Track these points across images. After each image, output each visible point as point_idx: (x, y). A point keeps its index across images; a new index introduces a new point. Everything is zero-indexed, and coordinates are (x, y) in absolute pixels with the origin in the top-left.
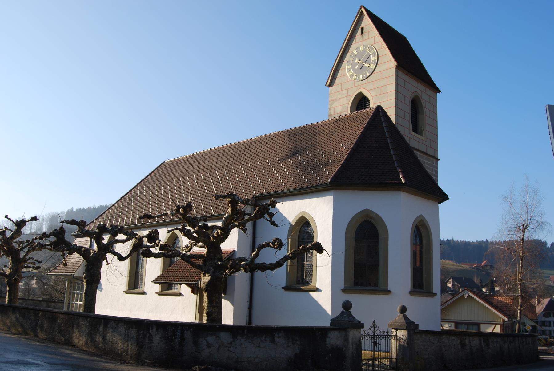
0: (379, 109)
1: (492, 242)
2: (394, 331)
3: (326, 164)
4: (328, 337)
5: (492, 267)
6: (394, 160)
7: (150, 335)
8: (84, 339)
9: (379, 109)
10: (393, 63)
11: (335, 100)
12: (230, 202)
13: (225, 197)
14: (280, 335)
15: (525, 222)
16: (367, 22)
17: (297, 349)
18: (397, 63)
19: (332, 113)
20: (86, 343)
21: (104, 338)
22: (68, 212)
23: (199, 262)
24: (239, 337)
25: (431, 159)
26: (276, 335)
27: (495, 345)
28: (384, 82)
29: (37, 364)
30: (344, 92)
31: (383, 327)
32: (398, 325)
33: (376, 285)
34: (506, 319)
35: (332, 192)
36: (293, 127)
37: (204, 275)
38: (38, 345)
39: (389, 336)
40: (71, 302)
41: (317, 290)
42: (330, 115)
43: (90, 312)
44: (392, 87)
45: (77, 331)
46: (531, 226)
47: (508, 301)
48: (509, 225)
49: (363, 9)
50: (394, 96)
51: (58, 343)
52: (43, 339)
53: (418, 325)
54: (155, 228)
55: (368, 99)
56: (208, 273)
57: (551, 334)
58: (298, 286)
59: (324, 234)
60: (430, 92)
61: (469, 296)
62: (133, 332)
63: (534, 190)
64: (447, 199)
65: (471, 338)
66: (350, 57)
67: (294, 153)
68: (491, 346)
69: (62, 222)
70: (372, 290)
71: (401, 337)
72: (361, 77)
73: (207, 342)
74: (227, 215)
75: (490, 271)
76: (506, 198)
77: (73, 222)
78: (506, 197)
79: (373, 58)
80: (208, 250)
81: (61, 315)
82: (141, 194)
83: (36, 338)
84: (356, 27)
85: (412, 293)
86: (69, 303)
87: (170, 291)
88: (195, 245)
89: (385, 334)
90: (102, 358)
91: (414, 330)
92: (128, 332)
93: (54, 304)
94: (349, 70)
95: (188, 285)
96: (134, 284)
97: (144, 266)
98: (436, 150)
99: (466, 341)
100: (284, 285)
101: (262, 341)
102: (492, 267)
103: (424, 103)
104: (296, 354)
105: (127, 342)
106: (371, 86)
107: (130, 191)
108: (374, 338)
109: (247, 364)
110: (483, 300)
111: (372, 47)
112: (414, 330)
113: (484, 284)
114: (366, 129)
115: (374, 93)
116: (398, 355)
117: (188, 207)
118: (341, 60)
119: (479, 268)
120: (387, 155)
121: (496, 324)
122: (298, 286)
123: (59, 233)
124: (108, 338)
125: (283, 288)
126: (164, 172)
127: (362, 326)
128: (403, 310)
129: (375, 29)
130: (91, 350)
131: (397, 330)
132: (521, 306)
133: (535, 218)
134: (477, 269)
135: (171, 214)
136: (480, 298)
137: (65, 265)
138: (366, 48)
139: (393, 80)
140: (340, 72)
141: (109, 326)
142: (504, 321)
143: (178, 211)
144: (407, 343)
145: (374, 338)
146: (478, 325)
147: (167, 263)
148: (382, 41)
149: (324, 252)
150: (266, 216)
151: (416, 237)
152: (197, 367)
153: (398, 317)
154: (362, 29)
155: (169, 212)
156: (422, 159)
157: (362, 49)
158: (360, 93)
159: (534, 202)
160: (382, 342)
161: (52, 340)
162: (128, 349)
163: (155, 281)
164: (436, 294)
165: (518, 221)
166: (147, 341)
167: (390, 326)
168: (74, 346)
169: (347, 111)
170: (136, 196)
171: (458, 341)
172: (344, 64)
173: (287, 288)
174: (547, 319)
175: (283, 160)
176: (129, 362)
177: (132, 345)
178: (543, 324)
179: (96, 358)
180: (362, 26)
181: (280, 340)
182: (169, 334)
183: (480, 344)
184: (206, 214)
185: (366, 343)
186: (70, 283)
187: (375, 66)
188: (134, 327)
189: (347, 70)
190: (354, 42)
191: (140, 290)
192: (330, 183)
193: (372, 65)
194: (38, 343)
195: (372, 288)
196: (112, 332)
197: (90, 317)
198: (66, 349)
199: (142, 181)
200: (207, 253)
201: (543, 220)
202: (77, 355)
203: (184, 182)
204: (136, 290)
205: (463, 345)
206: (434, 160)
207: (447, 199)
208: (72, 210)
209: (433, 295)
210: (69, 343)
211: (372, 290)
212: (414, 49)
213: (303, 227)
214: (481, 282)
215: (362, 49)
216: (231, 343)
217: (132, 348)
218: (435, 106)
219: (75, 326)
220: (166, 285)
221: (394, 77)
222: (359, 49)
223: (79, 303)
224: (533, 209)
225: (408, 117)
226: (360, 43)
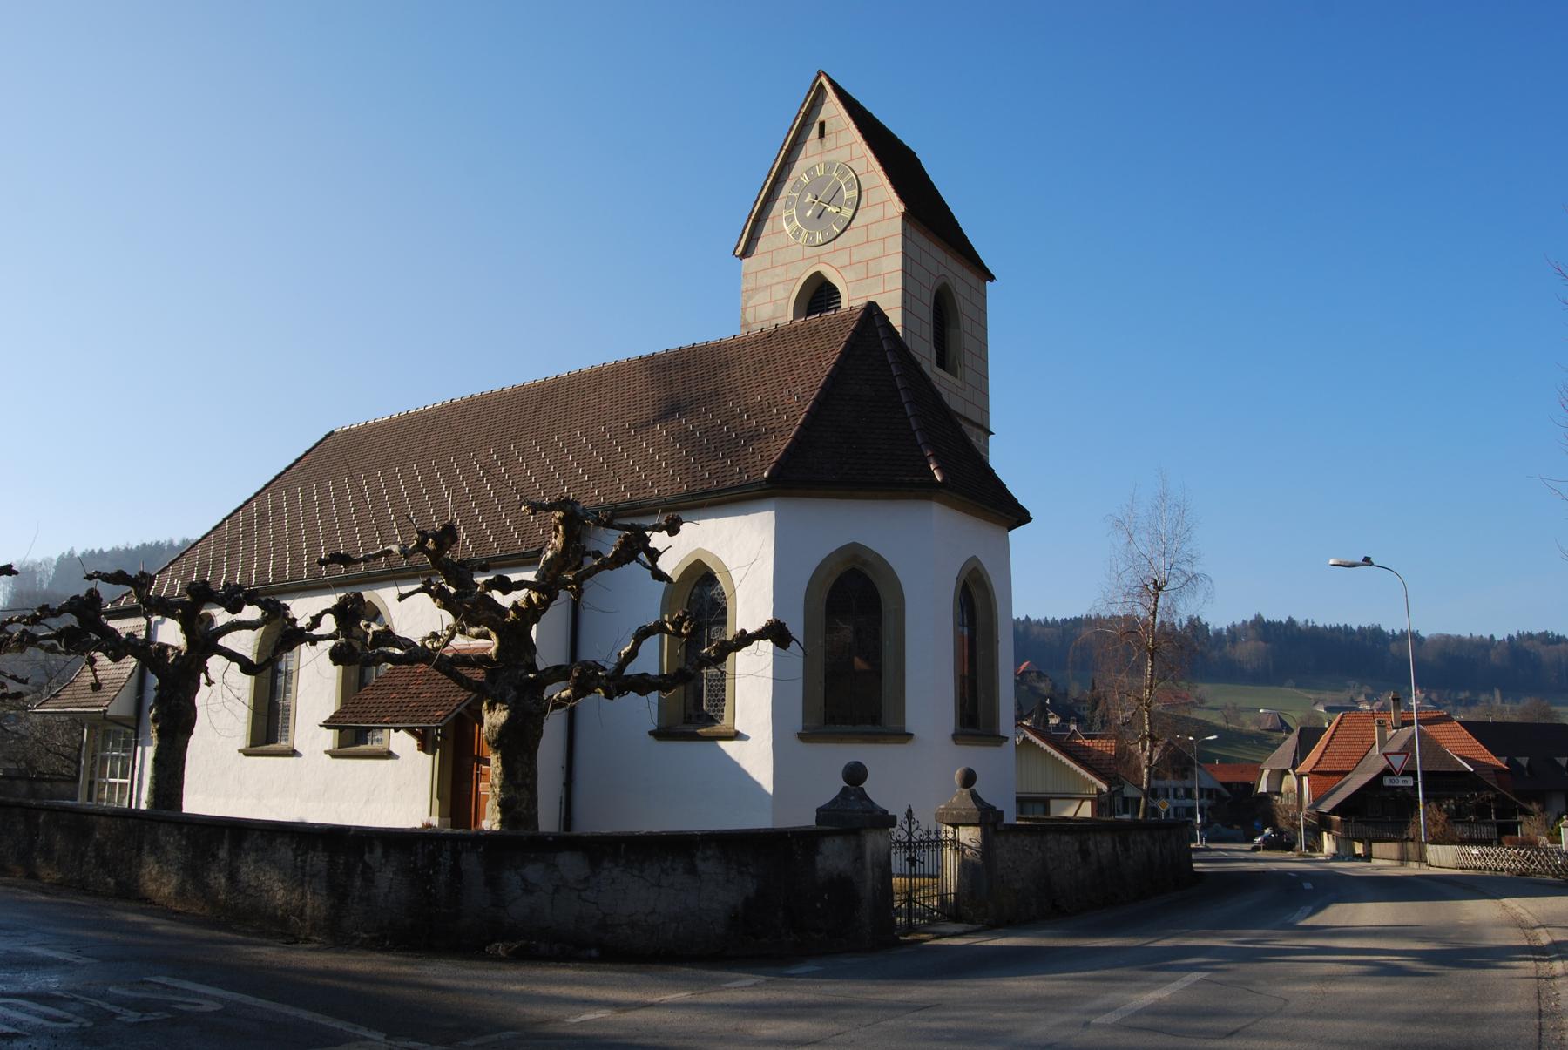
2: (950, 829)
3: (754, 436)
5: (1040, 675)
7: (367, 866)
8: (174, 882)
9: (872, 310)
10: (897, 207)
11: (756, 290)
12: (562, 521)
13: (551, 508)
14: (709, 853)
16: (833, 109)
19: (750, 317)
20: (181, 892)
21: (233, 878)
22: (61, 558)
23: (478, 675)
24: (606, 864)
28: (876, 249)
29: (65, 963)
30: (779, 271)
31: (926, 821)
32: (959, 815)
33: (876, 719)
34: (1105, 788)
35: (772, 502)
36: (659, 349)
37: (492, 707)
38: (45, 903)
39: (938, 843)
40: (97, 780)
41: (737, 736)
42: (745, 324)
43: (169, 808)
44: (895, 262)
45: (151, 860)
46: (1172, 584)
48: (1126, 580)
49: (823, 79)
51: (96, 894)
52: (51, 884)
53: (1001, 812)
54: (356, 589)
56: (502, 702)
58: (690, 728)
59: (751, 605)
60: (972, 278)
61: (1026, 740)
62: (318, 860)
64: (1030, 520)
66: (793, 189)
67: (670, 410)
69: (90, 577)
71: (967, 842)
72: (819, 238)
73: (524, 879)
74: (549, 554)
76: (1119, 524)
77: (119, 578)
79: (849, 194)
80: (501, 642)
81: (103, 820)
82: (277, 509)
83: (33, 883)
84: (808, 120)
85: (957, 737)
86: (91, 783)
87: (362, 747)
88: (463, 632)
89: (933, 837)
90: (235, 931)
92: (304, 861)
93: (48, 785)
94: (790, 220)
95: (411, 731)
96: (268, 730)
97: (293, 687)
98: (985, 411)
100: (654, 728)
102: (1040, 675)
103: (959, 300)
105: (302, 884)
106: (843, 259)
107: (247, 502)
108: (909, 848)
111: (845, 168)
116: (958, 887)
117: (448, 535)
120: (884, 415)
121: (1083, 800)
122: (690, 728)
123: (87, 608)
124: (243, 878)
125: (651, 733)
126: (335, 456)
127: (892, 821)
128: (969, 779)
129: (852, 126)
130: (195, 910)
131: (955, 826)
135: (402, 552)
136: (1049, 742)
137: (97, 686)
138: (831, 170)
139: (896, 245)
140: (768, 223)
141: (246, 845)
142: (1099, 790)
143: (421, 546)
144: (982, 857)
145: (909, 848)
146: (1044, 802)
147: (354, 677)
148: (870, 155)
149: (793, 644)
150: (643, 556)
152: (500, 945)
153: (959, 798)
154: (822, 125)
155: (395, 548)
157: (820, 173)
158: (818, 276)
160: (925, 856)
161: (82, 887)
162: (305, 905)
163: (328, 725)
166: (358, 883)
167: (941, 818)
168: (145, 902)
169: (785, 315)
170: (263, 515)
171: (1077, 846)
172: (779, 205)
173: (661, 734)
174: (1161, 783)
175: (642, 427)
176: (307, 940)
177: (314, 893)
179: (217, 934)
180: (821, 117)
182: (420, 863)
184: (487, 548)
185: (898, 861)
186: (92, 728)
188: (320, 846)
189: (784, 222)
190: (802, 155)
191: (282, 745)
192: (768, 480)
194: (43, 898)
195: (869, 728)
196: (256, 862)
197: (169, 821)
198: (126, 910)
199: (278, 477)
200: (499, 650)
201: (1196, 570)
202: (163, 927)
203: (390, 482)
204: (272, 747)
205: (1085, 853)
207: (1030, 520)
208: (71, 555)
210: (130, 893)
213: (702, 591)
215: (820, 173)
216: (586, 879)
217: (315, 902)
218: (983, 311)
219: (146, 848)
220: (353, 733)
221: (899, 239)
223: (118, 781)
225: (928, 332)
226: (816, 159)
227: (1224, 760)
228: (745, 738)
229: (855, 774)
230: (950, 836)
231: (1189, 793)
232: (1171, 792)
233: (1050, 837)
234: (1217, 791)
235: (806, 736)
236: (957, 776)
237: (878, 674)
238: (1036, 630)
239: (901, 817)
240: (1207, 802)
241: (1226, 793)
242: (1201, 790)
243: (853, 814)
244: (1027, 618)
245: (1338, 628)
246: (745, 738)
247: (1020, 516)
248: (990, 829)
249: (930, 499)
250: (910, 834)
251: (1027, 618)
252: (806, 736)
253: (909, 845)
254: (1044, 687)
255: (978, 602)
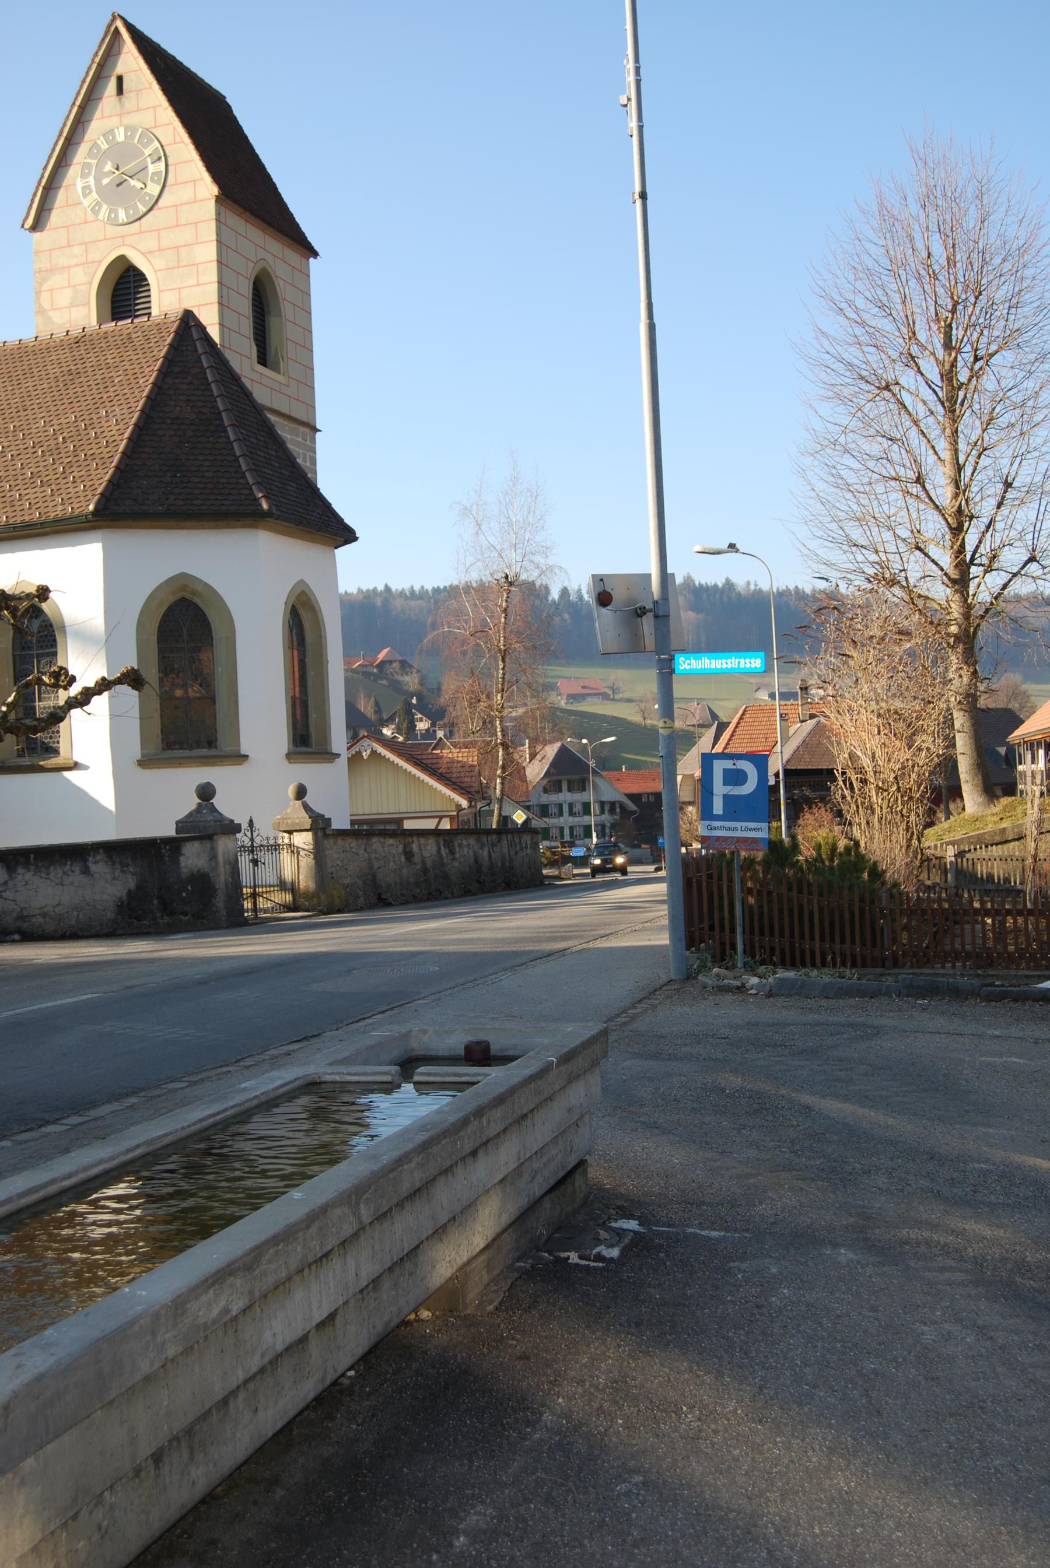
0: (188, 321)
1: (402, 593)
2: (286, 835)
4: (182, 855)
5: (405, 665)
6: (238, 453)
10: (209, 189)
11: (52, 271)
14: (99, 857)
15: (510, 567)
16: (131, 62)
17: (132, 883)
18: (220, 187)
24: (20, 870)
25: (302, 429)
26: (91, 859)
27: (466, 850)
28: (184, 236)
30: (76, 250)
31: (265, 831)
33: (211, 743)
34: (464, 803)
35: (98, 534)
39: (276, 848)
41: (75, 766)
44: (208, 252)
47: (470, 757)
49: (119, 24)
50: (213, 276)
55: (142, 274)
57: (562, 837)
58: (26, 761)
60: (292, 256)
61: (374, 753)
63: (529, 490)
64: (356, 539)
65: (422, 840)
66: (90, 154)
68: (457, 855)
70: (207, 757)
71: (301, 845)
72: (122, 216)
75: (400, 678)
76: (466, 512)
78: (465, 508)
85: (290, 756)
89: (272, 842)
91: (324, 829)
99: (414, 846)
101: (64, 873)
102: (405, 665)
104: (129, 891)
106: (150, 243)
108: (252, 852)
109: (42, 920)
110: (407, 760)
111: (149, 135)
112: (324, 829)
113: (385, 716)
114: (164, 373)
115: (159, 263)
118: (63, 161)
119: (369, 669)
122: (26, 761)
128: (301, 792)
132: (504, 768)
133: (532, 557)
134: (364, 673)
138: (133, 136)
145: (252, 852)
146: (399, 821)
149: (146, 686)
151: (291, 631)
154: (120, 79)
156: (284, 430)
157: (120, 137)
158: (122, 258)
159: (530, 519)
164: (338, 755)
165: (495, 567)
167: (277, 827)
171: (401, 848)
174: (554, 798)
178: (544, 811)
180: (119, 70)
181: (99, 867)
183: (439, 850)
185: (244, 861)
187: (158, 188)
190: (98, 114)
193: (149, 184)
195: (205, 751)
201: (551, 561)
205: (409, 854)
206: (307, 430)
207: (356, 539)
209: (333, 757)
211: (207, 757)
212: (264, 160)
214: (378, 710)
216: (6, 883)
221: (213, 225)
222: (114, 137)
224: (527, 535)
225: (247, 326)
226: (115, 121)
227: (633, 766)
228: (85, 768)
229: (206, 793)
230: (286, 841)
231: (586, 809)
232: (566, 808)
233: (375, 840)
234: (622, 806)
235: (145, 762)
236: (291, 791)
237: (213, 700)
238: (399, 603)
239: (245, 825)
240: (606, 818)
241: (632, 806)
242: (602, 804)
243: (206, 825)
244: (387, 588)
245: (788, 590)
246: (85, 768)
247: (346, 535)
248: (320, 834)
249: (256, 527)
250: (252, 840)
251: (387, 588)
252: (145, 762)
253: (252, 850)
254: (411, 681)
255: (307, 626)
